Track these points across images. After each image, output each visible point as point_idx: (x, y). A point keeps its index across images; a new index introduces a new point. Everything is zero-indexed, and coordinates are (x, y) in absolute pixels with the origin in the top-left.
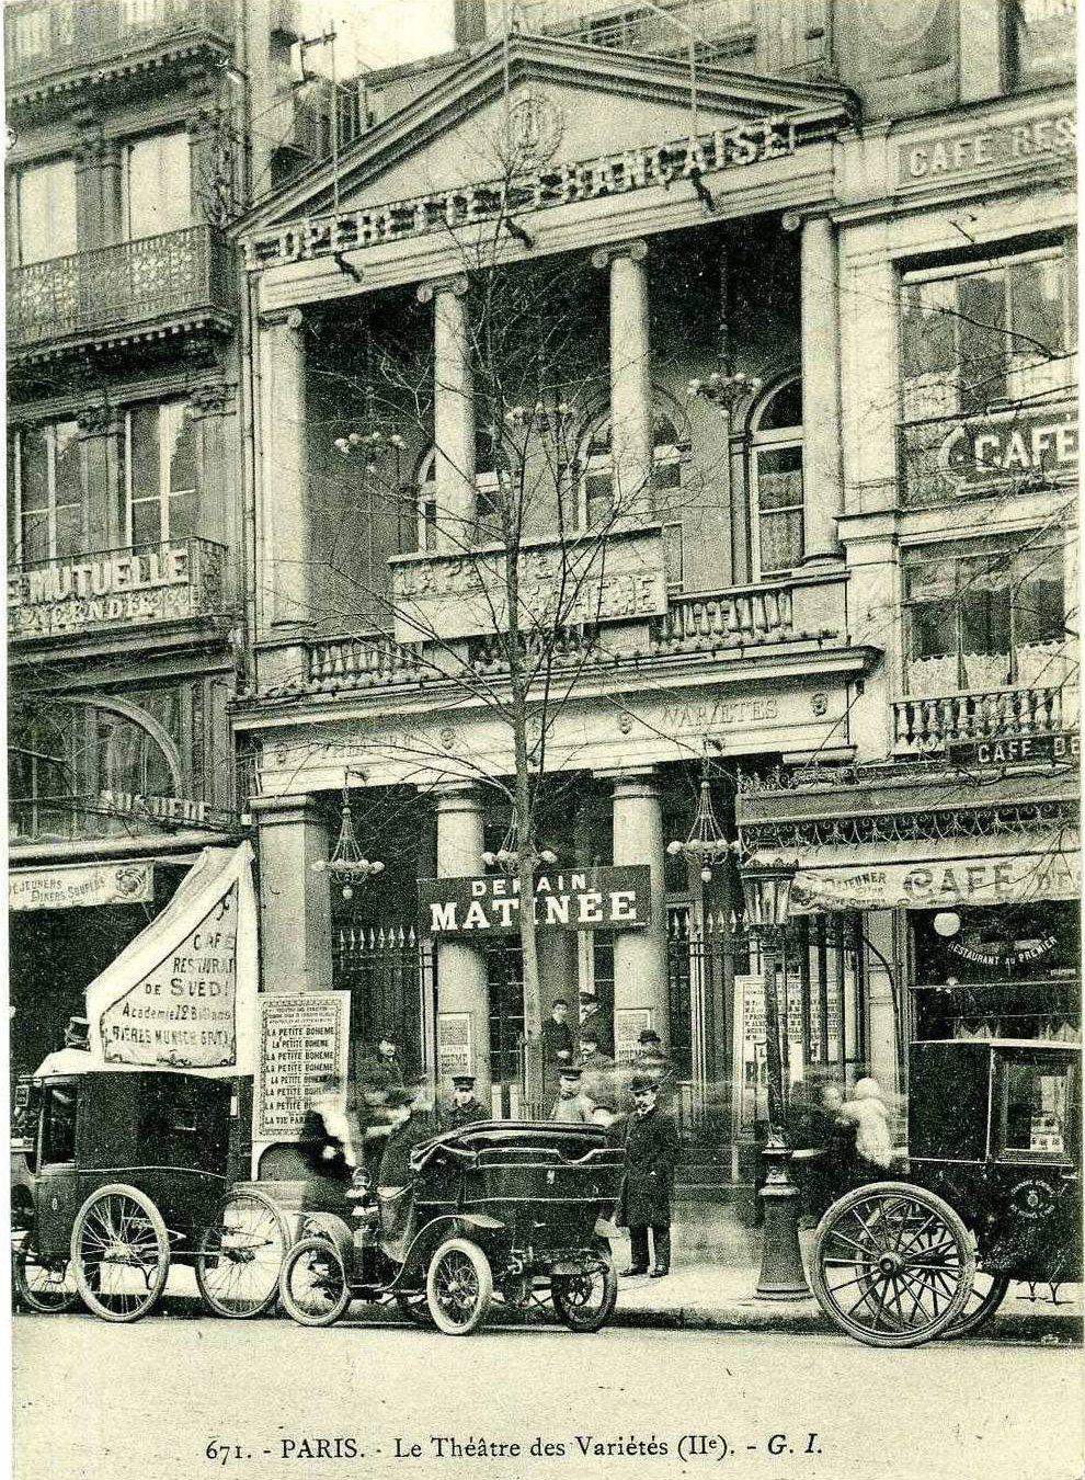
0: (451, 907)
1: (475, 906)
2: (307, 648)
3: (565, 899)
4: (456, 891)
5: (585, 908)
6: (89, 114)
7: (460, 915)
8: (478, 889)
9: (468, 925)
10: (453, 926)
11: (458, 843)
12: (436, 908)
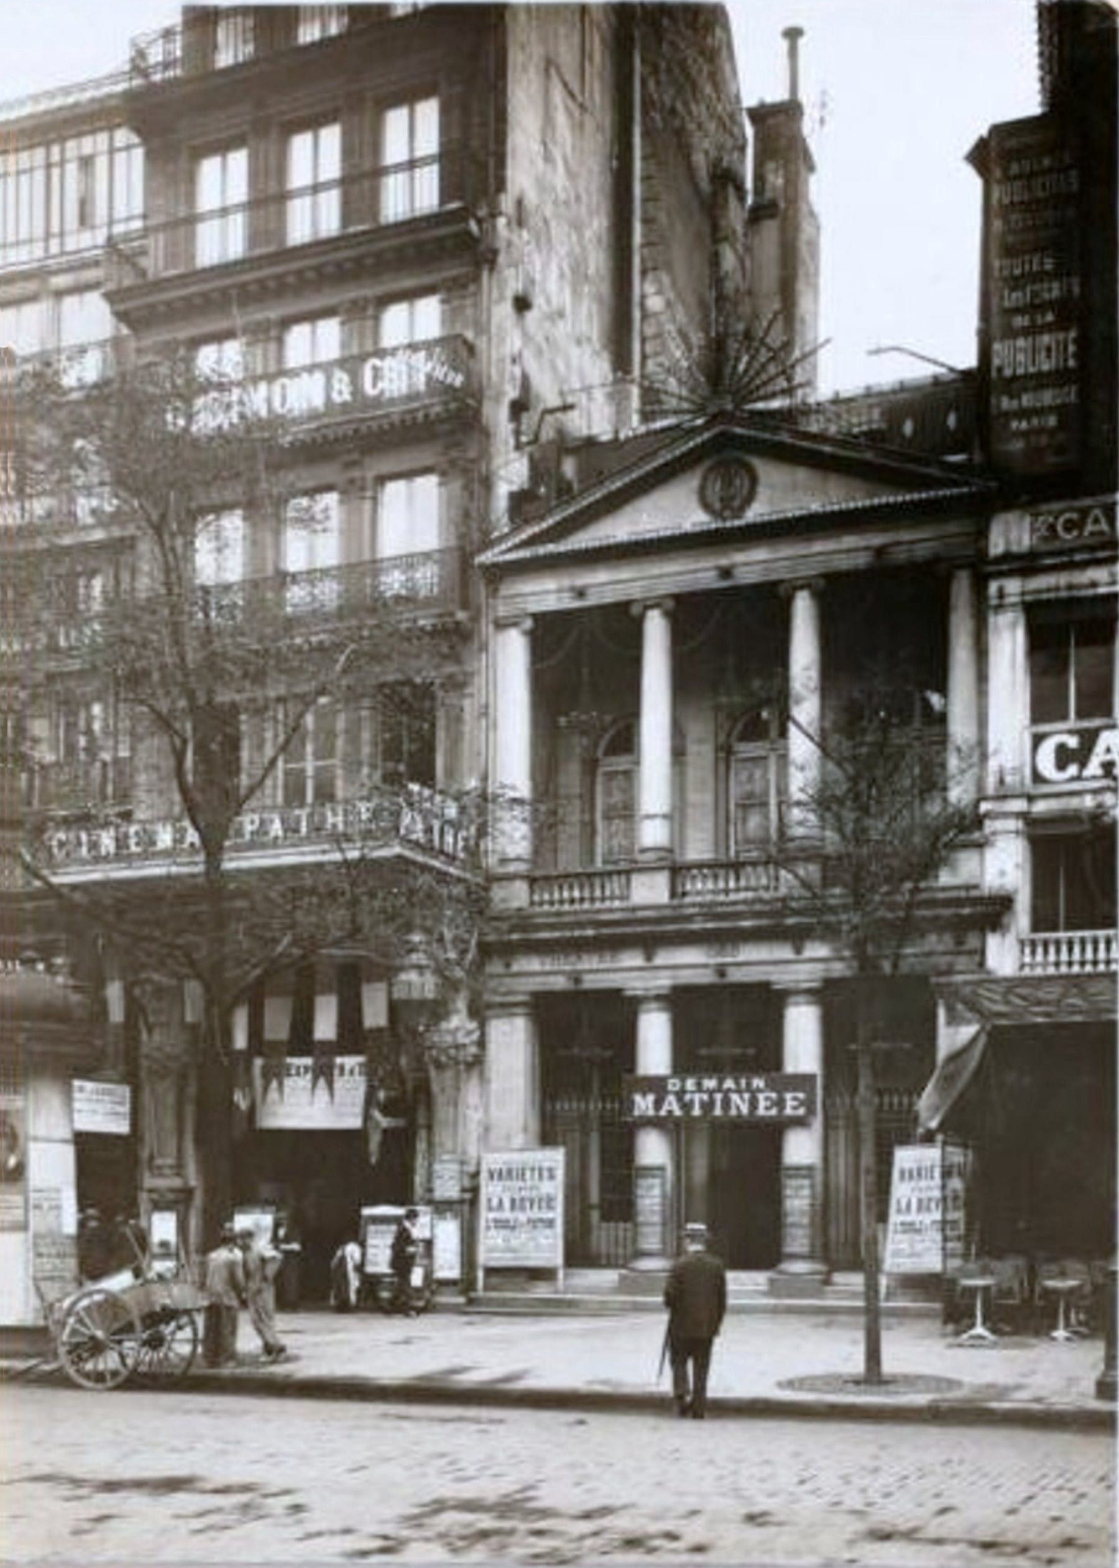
0: (651, 1098)
1: (671, 1098)
2: (532, 881)
3: (746, 1096)
4: (656, 1085)
5: (762, 1104)
6: (355, 456)
7: (658, 1104)
8: (673, 1085)
9: (663, 1113)
10: (651, 1112)
11: (654, 1043)
12: (638, 1098)
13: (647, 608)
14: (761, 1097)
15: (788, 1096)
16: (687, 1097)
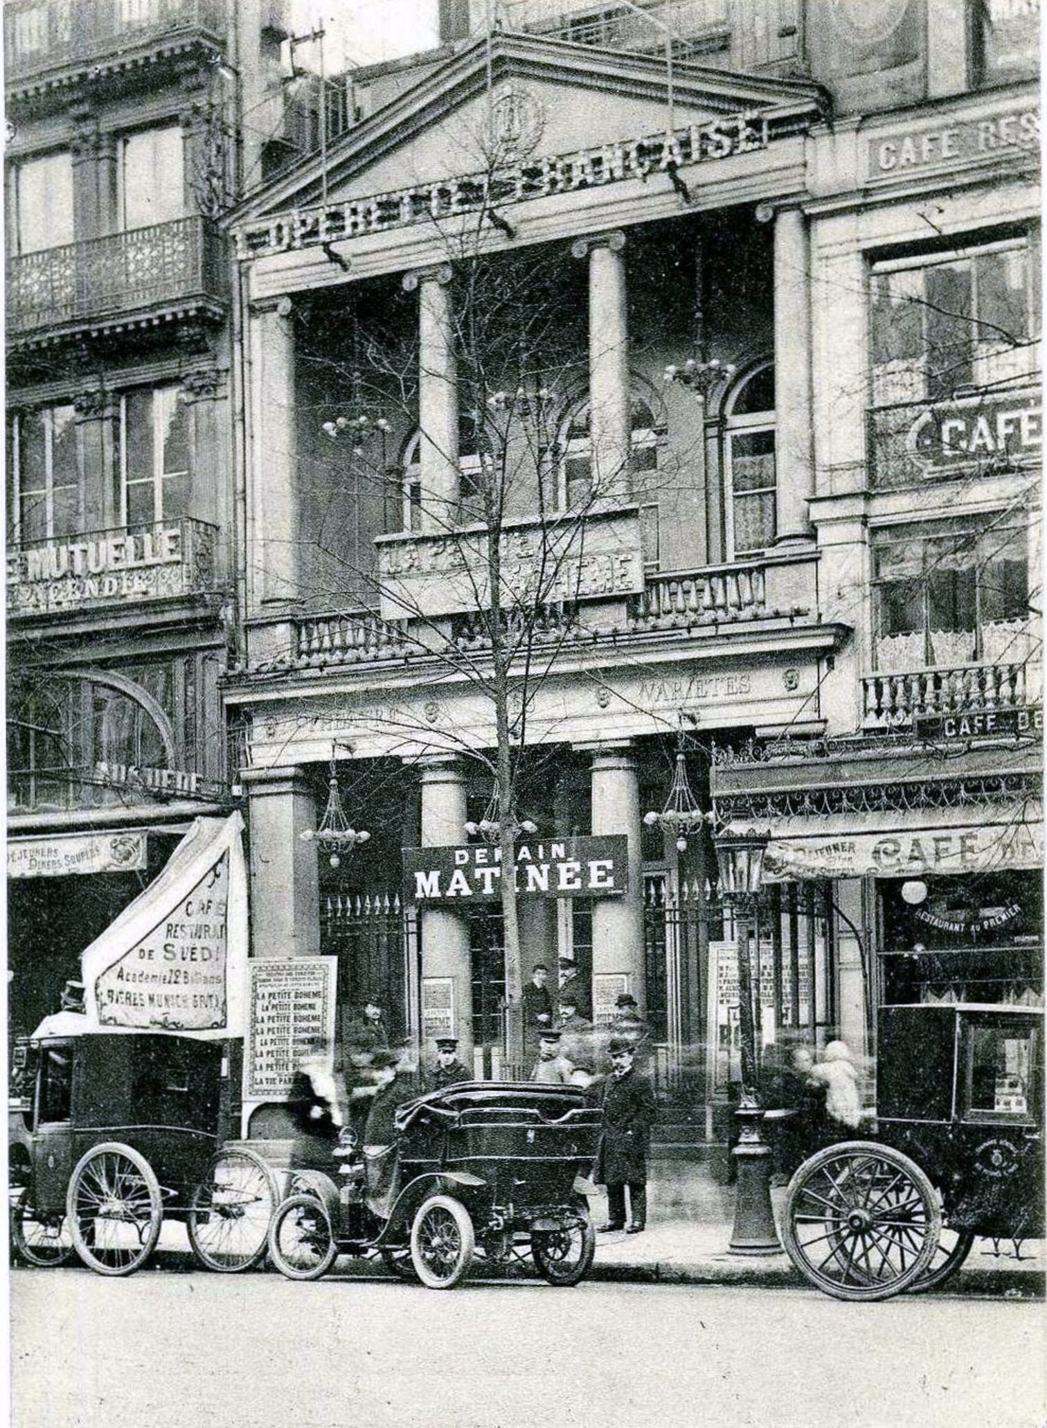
0: (434, 875)
1: (458, 874)
2: (296, 624)
4: (440, 860)
5: (564, 876)
7: (444, 883)
8: (461, 857)
9: (451, 893)
10: (436, 893)
11: (441, 813)
12: (420, 876)
13: (592, 246)
14: (562, 867)
15: (593, 865)
16: (478, 873)
